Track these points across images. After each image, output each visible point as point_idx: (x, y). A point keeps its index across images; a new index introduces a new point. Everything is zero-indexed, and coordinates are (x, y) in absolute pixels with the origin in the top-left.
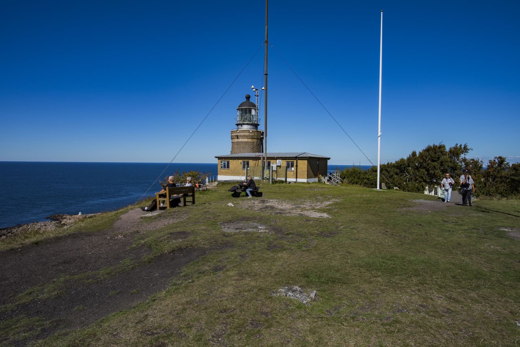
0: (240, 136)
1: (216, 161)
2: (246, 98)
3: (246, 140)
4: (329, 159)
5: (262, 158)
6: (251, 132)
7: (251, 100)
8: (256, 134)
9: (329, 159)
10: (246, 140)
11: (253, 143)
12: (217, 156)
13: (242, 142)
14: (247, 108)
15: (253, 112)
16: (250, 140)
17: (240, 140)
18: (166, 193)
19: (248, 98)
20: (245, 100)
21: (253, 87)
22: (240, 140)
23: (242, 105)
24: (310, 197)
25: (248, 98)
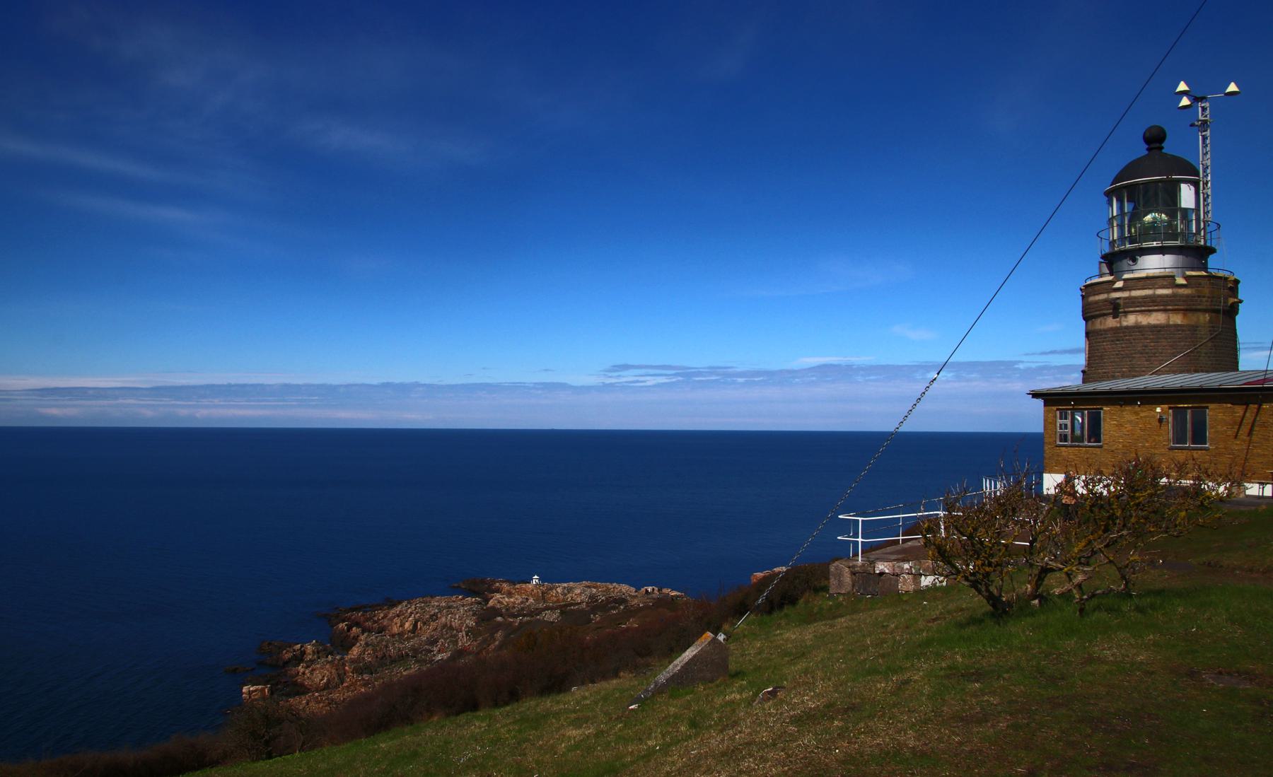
0: (1132, 302)
1: (1032, 418)
2: (1147, 140)
3: (1157, 318)
7: (1169, 147)
8: (1206, 291)
10: (1157, 318)
11: (1194, 328)
13: (1138, 328)
15: (1187, 197)
16: (1177, 319)
17: (1131, 320)
19: (1155, 139)
20: (1141, 150)
22: (1131, 320)
25: (1155, 139)
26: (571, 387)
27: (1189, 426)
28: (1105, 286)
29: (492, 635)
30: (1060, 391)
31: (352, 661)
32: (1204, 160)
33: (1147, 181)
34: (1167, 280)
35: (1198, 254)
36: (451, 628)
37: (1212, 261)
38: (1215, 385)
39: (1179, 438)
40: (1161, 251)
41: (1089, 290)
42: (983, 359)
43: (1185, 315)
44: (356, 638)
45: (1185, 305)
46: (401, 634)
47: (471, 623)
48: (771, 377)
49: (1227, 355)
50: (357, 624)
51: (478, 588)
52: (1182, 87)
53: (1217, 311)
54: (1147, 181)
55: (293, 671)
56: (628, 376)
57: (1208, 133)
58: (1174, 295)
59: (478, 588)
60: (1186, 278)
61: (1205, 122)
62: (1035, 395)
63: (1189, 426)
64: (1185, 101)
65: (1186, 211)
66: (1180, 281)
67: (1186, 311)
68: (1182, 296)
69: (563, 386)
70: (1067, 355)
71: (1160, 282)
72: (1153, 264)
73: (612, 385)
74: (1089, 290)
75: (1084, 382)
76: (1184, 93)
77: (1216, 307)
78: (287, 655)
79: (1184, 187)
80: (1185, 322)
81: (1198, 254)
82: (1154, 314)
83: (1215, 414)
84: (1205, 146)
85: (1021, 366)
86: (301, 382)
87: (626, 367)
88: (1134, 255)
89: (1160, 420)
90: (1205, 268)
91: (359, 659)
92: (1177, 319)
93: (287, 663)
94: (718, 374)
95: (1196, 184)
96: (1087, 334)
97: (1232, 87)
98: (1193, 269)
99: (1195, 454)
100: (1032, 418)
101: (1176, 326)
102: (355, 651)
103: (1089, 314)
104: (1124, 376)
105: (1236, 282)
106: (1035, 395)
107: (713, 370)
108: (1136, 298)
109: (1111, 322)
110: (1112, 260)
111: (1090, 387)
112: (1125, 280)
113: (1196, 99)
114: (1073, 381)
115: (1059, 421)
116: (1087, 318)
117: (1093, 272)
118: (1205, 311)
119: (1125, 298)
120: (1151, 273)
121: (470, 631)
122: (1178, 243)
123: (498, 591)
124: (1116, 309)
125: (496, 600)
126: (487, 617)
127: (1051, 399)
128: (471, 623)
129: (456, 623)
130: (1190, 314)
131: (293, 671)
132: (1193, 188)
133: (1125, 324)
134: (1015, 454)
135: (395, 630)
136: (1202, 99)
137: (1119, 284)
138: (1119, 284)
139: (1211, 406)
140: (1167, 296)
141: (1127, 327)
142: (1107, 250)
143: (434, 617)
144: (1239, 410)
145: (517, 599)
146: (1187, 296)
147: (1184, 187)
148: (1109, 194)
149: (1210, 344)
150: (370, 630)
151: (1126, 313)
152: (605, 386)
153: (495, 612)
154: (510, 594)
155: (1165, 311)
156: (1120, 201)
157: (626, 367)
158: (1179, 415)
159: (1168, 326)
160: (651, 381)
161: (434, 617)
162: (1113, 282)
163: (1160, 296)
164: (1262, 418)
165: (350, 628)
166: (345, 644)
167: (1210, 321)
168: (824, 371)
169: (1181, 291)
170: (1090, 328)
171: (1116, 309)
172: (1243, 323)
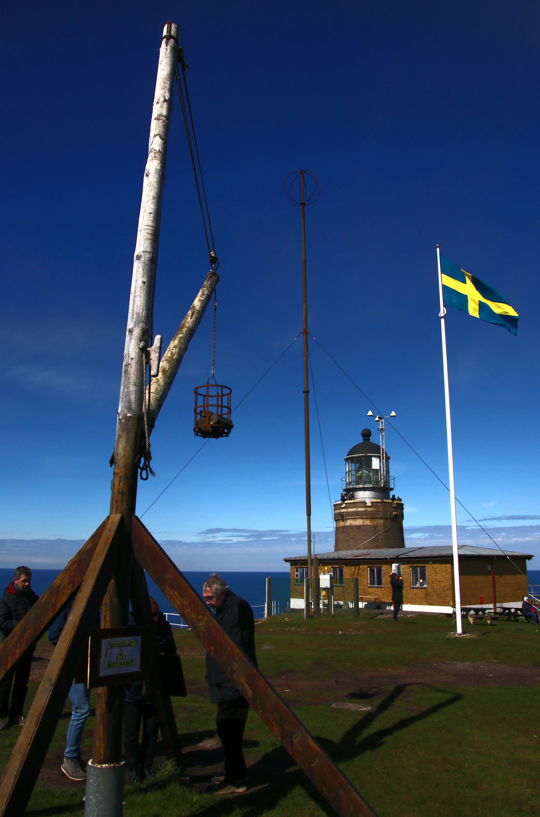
0: (348, 514)
1: (287, 568)
2: (363, 435)
3: (359, 522)
4: (530, 557)
5: (309, 562)
6: (369, 504)
7: (372, 439)
8: (381, 509)
9: (530, 557)
10: (359, 522)
11: (375, 527)
12: (288, 557)
13: (351, 527)
14: (360, 455)
15: (376, 464)
16: (368, 522)
17: (349, 523)
18: (454, 613)
19: (367, 435)
20: (360, 440)
21: (370, 413)
22: (349, 523)
23: (351, 452)
24: (219, 686)
25: (367, 435)
26: (185, 544)
27: (376, 574)
28: (339, 506)
40: (364, 489)
43: (371, 521)
53: (387, 518)
56: (220, 537)
57: (384, 434)
58: (365, 511)
61: (382, 429)
62: (286, 561)
63: (376, 574)
64: (377, 419)
65: (376, 471)
67: (371, 519)
68: (370, 511)
70: (505, 521)
71: (360, 505)
76: (373, 416)
79: (373, 459)
80: (371, 524)
82: (358, 520)
84: (382, 438)
85: (469, 528)
92: (368, 522)
94: (278, 536)
97: (393, 414)
100: (287, 568)
101: (367, 526)
104: (346, 549)
106: (286, 561)
107: (273, 533)
108: (350, 512)
111: (336, 555)
112: (346, 504)
115: (296, 573)
118: (381, 518)
119: (346, 512)
127: (294, 562)
130: (373, 520)
132: (378, 460)
133: (346, 524)
137: (344, 506)
138: (344, 506)
139: (427, 565)
140: (362, 511)
141: (347, 526)
144: (353, 568)
146: (372, 511)
147: (373, 459)
148: (346, 460)
149: (383, 534)
151: (347, 519)
155: (362, 518)
159: (364, 526)
160: (235, 540)
162: (341, 504)
163: (360, 511)
164: (360, 572)
167: (384, 523)
170: (338, 526)
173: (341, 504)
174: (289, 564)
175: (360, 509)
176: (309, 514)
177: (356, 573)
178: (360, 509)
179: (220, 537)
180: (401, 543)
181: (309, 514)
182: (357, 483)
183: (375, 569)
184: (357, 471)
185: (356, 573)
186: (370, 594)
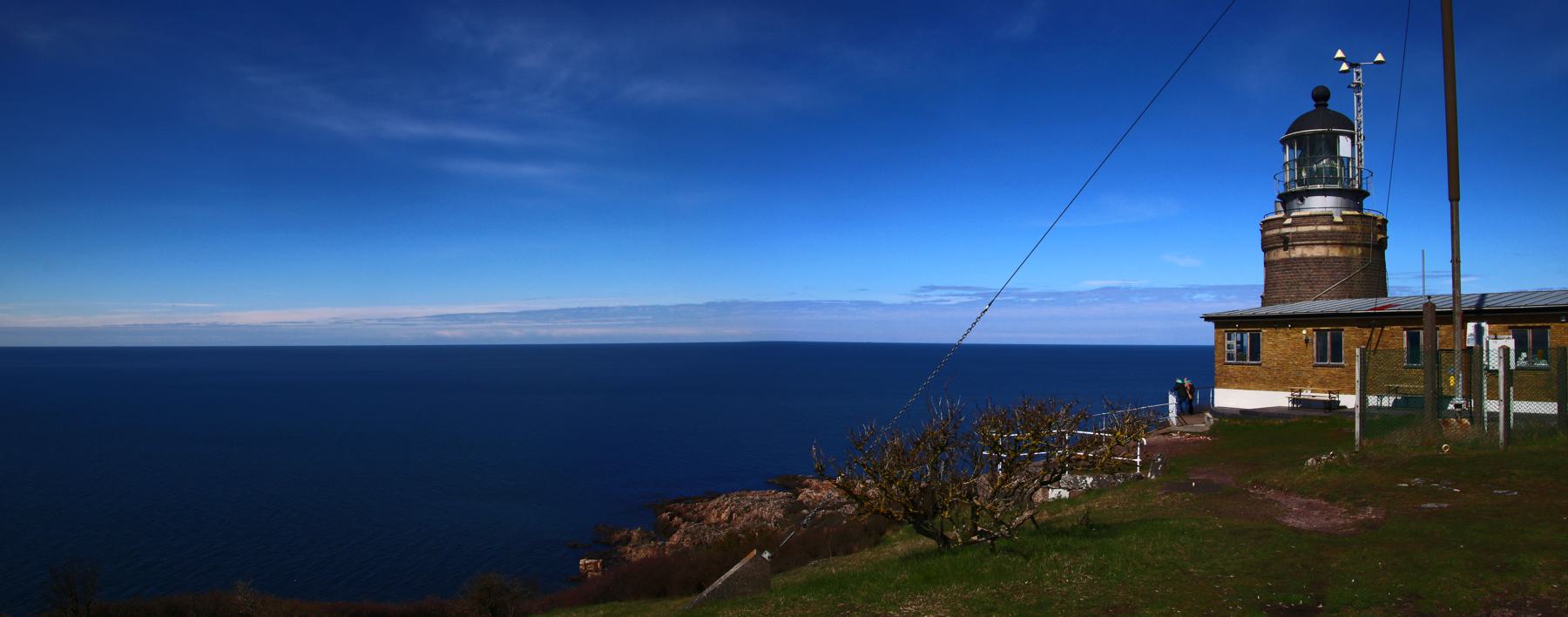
0: (1298, 236)
1: (1206, 335)
2: (1315, 98)
3: (1319, 251)
7: (1332, 105)
8: (1359, 228)
10: (1319, 251)
11: (1348, 260)
13: (1303, 259)
15: (1344, 147)
16: (1335, 252)
17: (1298, 252)
19: (1321, 97)
20: (1310, 106)
22: (1298, 252)
23: (1299, 123)
25: (1321, 97)
26: (883, 305)
29: (731, 516)
30: (1540, 303)
31: (672, 547)
32: (1358, 117)
33: (1313, 136)
34: (1327, 218)
35: (1355, 196)
36: (762, 519)
37: (1366, 203)
38: (1348, 310)
39: (1321, 357)
41: (1266, 225)
42: (1239, 283)
44: (678, 527)
45: (1342, 240)
46: (717, 524)
47: (779, 515)
48: (1059, 297)
49: (1375, 280)
50: (679, 515)
51: (791, 484)
52: (1340, 54)
53: (1367, 246)
54: (1313, 136)
55: (622, 550)
56: (934, 296)
59: (791, 484)
60: (1343, 216)
62: (1207, 318)
64: (1344, 67)
66: (1338, 219)
67: (1342, 245)
69: (876, 304)
72: (1318, 204)
73: (920, 303)
74: (1266, 225)
75: (1263, 304)
76: (1341, 60)
77: (1367, 244)
78: (617, 537)
81: (1355, 196)
83: (1349, 334)
86: (637, 304)
87: (933, 288)
88: (1302, 195)
89: (1307, 341)
90: (1360, 208)
91: (679, 544)
92: (1335, 252)
93: (617, 543)
95: (1352, 136)
96: (1266, 264)
97: (1380, 58)
98: (1348, 209)
99: (1333, 371)
100: (1206, 335)
102: (675, 538)
103: (1267, 246)
104: (1292, 301)
105: (1385, 221)
106: (1207, 318)
109: (1282, 254)
110: (1286, 199)
111: (1264, 311)
113: (1352, 66)
114: (1251, 304)
116: (1264, 250)
117: (1270, 209)
118: (1358, 245)
120: (1314, 212)
121: (778, 521)
122: (1338, 186)
123: (808, 486)
124: (1286, 242)
125: (806, 494)
126: (794, 509)
128: (779, 515)
129: (766, 514)
131: (622, 550)
134: (1188, 371)
135: (713, 520)
136: (1357, 65)
137: (1289, 221)
138: (1289, 221)
139: (1553, 325)
142: (1282, 190)
143: (748, 510)
144: (1367, 332)
145: (824, 494)
148: (1283, 142)
150: (690, 520)
151: (1294, 246)
152: (913, 304)
153: (801, 505)
154: (817, 490)
156: (1292, 147)
157: (933, 288)
158: (1321, 336)
160: (954, 301)
161: (748, 510)
162: (1283, 219)
164: (1384, 339)
165: (672, 518)
166: (668, 531)
168: (1106, 292)
169: (1338, 228)
171: (1286, 242)
172: (1389, 254)
173: (1283, 219)
174: (1211, 325)
175: (1322, 228)
176: (1454, 197)
177: (1374, 341)
178: (1322, 228)
179: (934, 296)
180: (1382, 291)
181: (1454, 197)
182: (1311, 180)
183: (1530, 332)
184: (1301, 163)
185: (1374, 341)
186: (1406, 380)
